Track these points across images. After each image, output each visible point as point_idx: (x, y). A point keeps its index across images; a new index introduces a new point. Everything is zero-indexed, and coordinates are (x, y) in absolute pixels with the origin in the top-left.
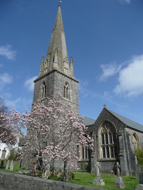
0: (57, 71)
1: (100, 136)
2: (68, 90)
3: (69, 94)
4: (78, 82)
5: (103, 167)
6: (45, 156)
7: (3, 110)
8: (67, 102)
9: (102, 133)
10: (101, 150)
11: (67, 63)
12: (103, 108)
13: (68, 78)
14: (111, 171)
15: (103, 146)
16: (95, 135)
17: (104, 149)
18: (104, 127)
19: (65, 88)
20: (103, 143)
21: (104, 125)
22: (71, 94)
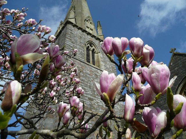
3: (98, 59)
19: (88, 49)
21: (15, 107)
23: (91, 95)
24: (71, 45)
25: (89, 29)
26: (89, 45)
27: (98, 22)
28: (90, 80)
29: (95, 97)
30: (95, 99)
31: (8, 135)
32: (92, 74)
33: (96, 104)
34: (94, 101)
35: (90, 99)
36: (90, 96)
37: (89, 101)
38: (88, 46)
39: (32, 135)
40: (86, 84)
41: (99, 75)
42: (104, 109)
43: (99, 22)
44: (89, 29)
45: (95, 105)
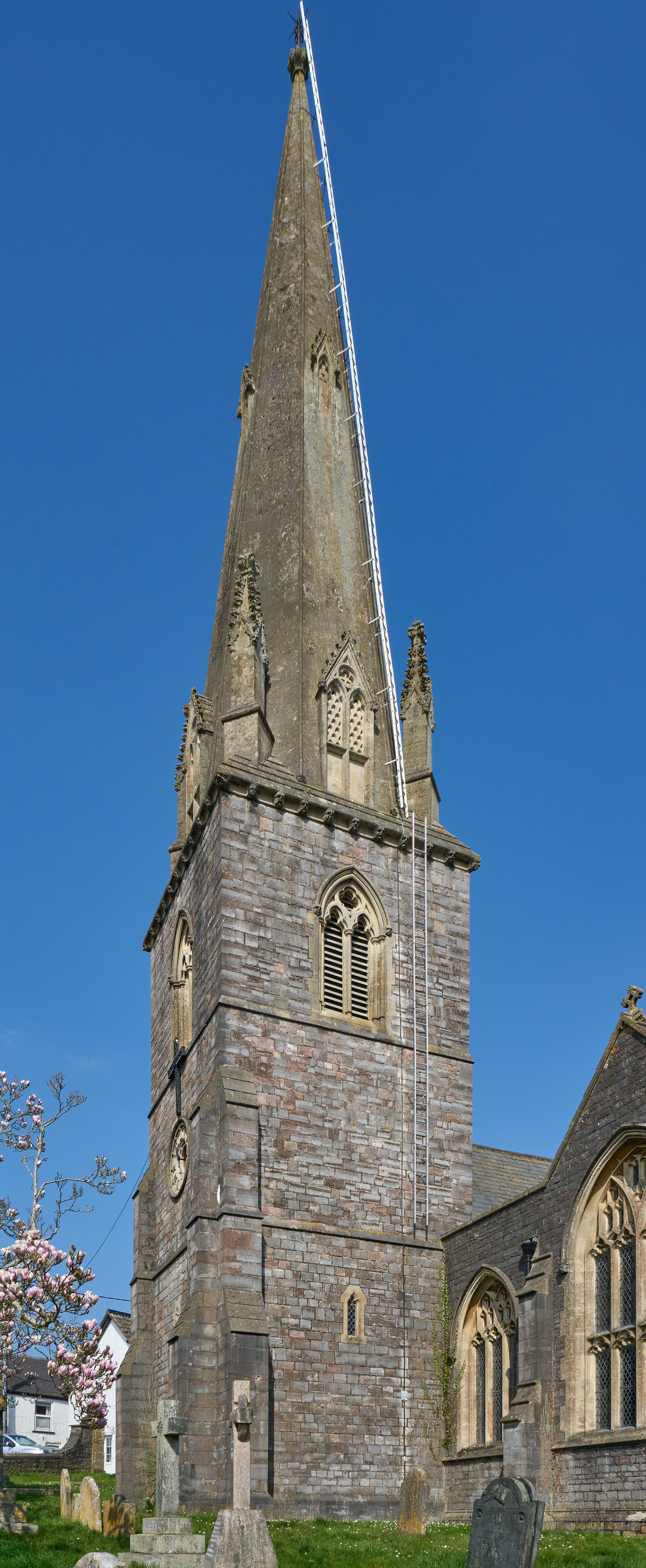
0: (243, 784)
1: (583, 1272)
2: (373, 950)
3: (381, 978)
4: (465, 860)
5: (583, 1488)
6: (239, 1547)
7: (2, 1437)
8: (351, 1042)
9: (601, 1243)
10: (587, 1368)
11: (357, 695)
12: (613, 1025)
13: (364, 841)
14: (631, 1517)
15: (601, 1340)
16: (548, 1268)
17: (604, 1361)
18: (616, 1190)
19: (332, 925)
20: (605, 1320)
21: (620, 1173)
22: (392, 976)
23: (338, 1167)
24: (249, 943)
25: (346, 755)
26: (337, 902)
27: (412, 638)
28: (335, 1103)
29: (353, 1172)
30: (355, 1178)
31: (235, 1382)
32: (342, 1075)
33: (353, 1198)
34: (348, 1187)
35: (331, 1183)
36: (328, 1173)
37: (328, 1192)
38: (335, 909)
39: (456, 1449)
40: (320, 1123)
41: (378, 1066)
42: (384, 1211)
43: (421, 636)
44: (346, 755)
45: (351, 1201)
